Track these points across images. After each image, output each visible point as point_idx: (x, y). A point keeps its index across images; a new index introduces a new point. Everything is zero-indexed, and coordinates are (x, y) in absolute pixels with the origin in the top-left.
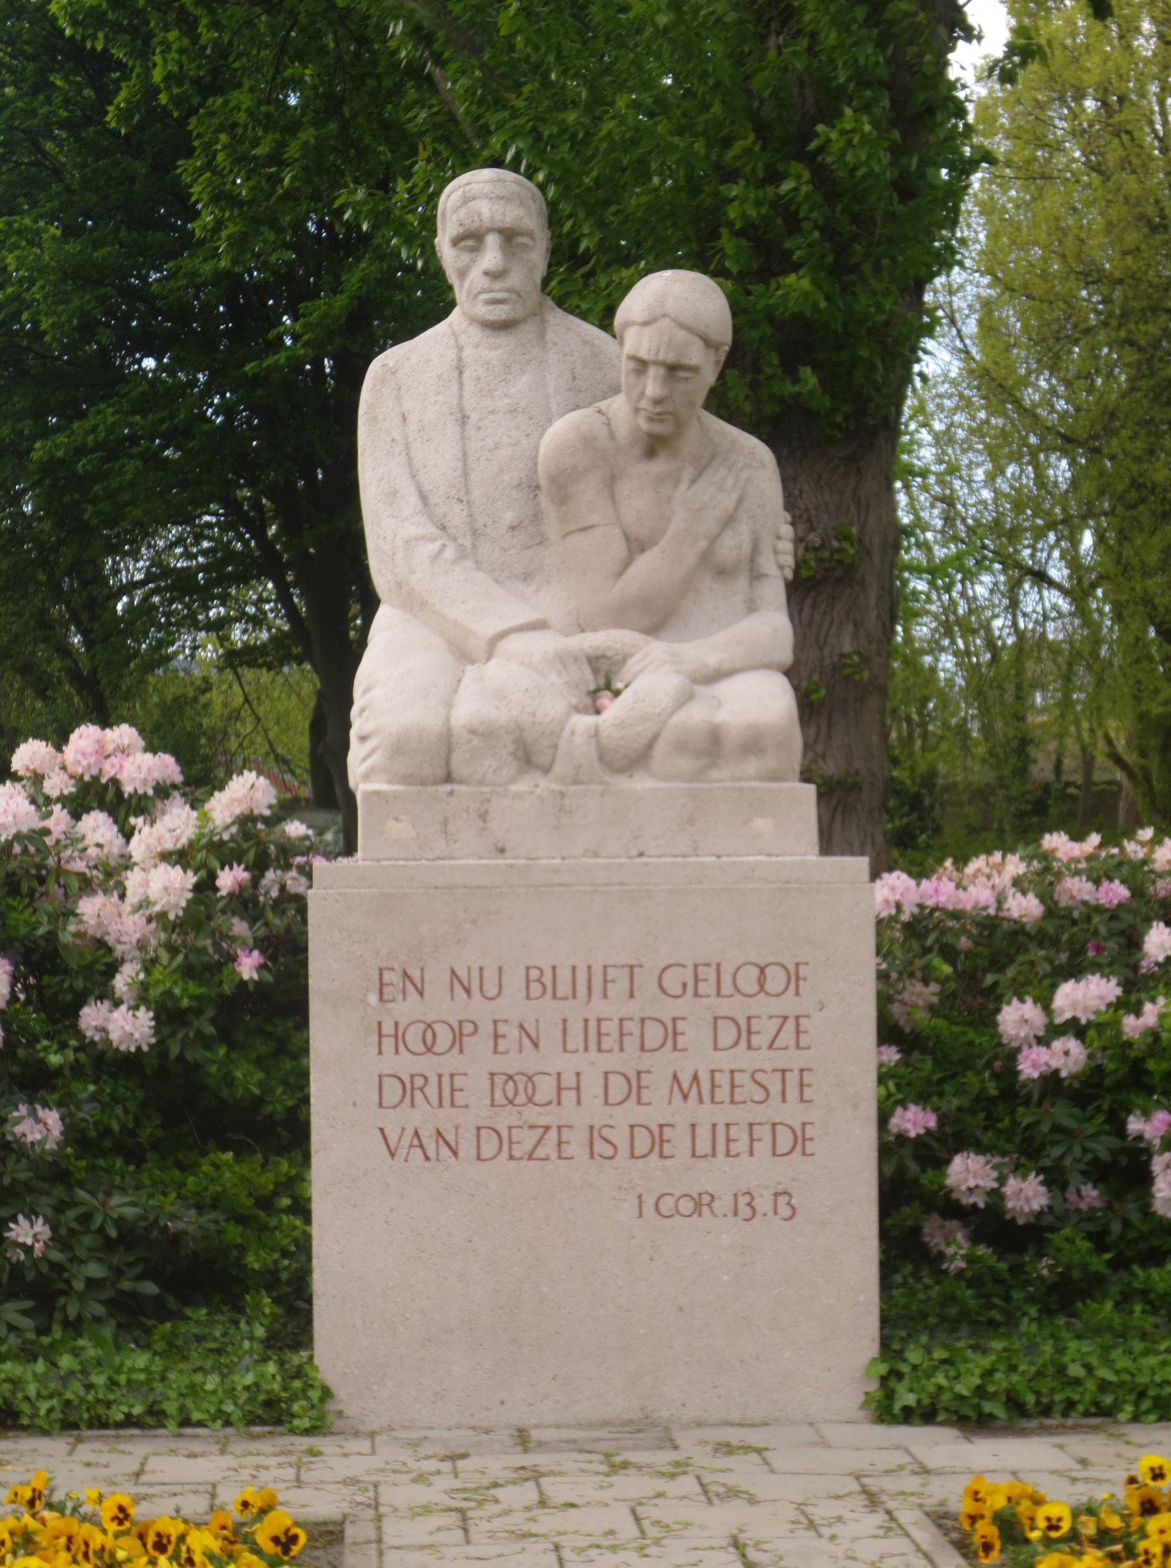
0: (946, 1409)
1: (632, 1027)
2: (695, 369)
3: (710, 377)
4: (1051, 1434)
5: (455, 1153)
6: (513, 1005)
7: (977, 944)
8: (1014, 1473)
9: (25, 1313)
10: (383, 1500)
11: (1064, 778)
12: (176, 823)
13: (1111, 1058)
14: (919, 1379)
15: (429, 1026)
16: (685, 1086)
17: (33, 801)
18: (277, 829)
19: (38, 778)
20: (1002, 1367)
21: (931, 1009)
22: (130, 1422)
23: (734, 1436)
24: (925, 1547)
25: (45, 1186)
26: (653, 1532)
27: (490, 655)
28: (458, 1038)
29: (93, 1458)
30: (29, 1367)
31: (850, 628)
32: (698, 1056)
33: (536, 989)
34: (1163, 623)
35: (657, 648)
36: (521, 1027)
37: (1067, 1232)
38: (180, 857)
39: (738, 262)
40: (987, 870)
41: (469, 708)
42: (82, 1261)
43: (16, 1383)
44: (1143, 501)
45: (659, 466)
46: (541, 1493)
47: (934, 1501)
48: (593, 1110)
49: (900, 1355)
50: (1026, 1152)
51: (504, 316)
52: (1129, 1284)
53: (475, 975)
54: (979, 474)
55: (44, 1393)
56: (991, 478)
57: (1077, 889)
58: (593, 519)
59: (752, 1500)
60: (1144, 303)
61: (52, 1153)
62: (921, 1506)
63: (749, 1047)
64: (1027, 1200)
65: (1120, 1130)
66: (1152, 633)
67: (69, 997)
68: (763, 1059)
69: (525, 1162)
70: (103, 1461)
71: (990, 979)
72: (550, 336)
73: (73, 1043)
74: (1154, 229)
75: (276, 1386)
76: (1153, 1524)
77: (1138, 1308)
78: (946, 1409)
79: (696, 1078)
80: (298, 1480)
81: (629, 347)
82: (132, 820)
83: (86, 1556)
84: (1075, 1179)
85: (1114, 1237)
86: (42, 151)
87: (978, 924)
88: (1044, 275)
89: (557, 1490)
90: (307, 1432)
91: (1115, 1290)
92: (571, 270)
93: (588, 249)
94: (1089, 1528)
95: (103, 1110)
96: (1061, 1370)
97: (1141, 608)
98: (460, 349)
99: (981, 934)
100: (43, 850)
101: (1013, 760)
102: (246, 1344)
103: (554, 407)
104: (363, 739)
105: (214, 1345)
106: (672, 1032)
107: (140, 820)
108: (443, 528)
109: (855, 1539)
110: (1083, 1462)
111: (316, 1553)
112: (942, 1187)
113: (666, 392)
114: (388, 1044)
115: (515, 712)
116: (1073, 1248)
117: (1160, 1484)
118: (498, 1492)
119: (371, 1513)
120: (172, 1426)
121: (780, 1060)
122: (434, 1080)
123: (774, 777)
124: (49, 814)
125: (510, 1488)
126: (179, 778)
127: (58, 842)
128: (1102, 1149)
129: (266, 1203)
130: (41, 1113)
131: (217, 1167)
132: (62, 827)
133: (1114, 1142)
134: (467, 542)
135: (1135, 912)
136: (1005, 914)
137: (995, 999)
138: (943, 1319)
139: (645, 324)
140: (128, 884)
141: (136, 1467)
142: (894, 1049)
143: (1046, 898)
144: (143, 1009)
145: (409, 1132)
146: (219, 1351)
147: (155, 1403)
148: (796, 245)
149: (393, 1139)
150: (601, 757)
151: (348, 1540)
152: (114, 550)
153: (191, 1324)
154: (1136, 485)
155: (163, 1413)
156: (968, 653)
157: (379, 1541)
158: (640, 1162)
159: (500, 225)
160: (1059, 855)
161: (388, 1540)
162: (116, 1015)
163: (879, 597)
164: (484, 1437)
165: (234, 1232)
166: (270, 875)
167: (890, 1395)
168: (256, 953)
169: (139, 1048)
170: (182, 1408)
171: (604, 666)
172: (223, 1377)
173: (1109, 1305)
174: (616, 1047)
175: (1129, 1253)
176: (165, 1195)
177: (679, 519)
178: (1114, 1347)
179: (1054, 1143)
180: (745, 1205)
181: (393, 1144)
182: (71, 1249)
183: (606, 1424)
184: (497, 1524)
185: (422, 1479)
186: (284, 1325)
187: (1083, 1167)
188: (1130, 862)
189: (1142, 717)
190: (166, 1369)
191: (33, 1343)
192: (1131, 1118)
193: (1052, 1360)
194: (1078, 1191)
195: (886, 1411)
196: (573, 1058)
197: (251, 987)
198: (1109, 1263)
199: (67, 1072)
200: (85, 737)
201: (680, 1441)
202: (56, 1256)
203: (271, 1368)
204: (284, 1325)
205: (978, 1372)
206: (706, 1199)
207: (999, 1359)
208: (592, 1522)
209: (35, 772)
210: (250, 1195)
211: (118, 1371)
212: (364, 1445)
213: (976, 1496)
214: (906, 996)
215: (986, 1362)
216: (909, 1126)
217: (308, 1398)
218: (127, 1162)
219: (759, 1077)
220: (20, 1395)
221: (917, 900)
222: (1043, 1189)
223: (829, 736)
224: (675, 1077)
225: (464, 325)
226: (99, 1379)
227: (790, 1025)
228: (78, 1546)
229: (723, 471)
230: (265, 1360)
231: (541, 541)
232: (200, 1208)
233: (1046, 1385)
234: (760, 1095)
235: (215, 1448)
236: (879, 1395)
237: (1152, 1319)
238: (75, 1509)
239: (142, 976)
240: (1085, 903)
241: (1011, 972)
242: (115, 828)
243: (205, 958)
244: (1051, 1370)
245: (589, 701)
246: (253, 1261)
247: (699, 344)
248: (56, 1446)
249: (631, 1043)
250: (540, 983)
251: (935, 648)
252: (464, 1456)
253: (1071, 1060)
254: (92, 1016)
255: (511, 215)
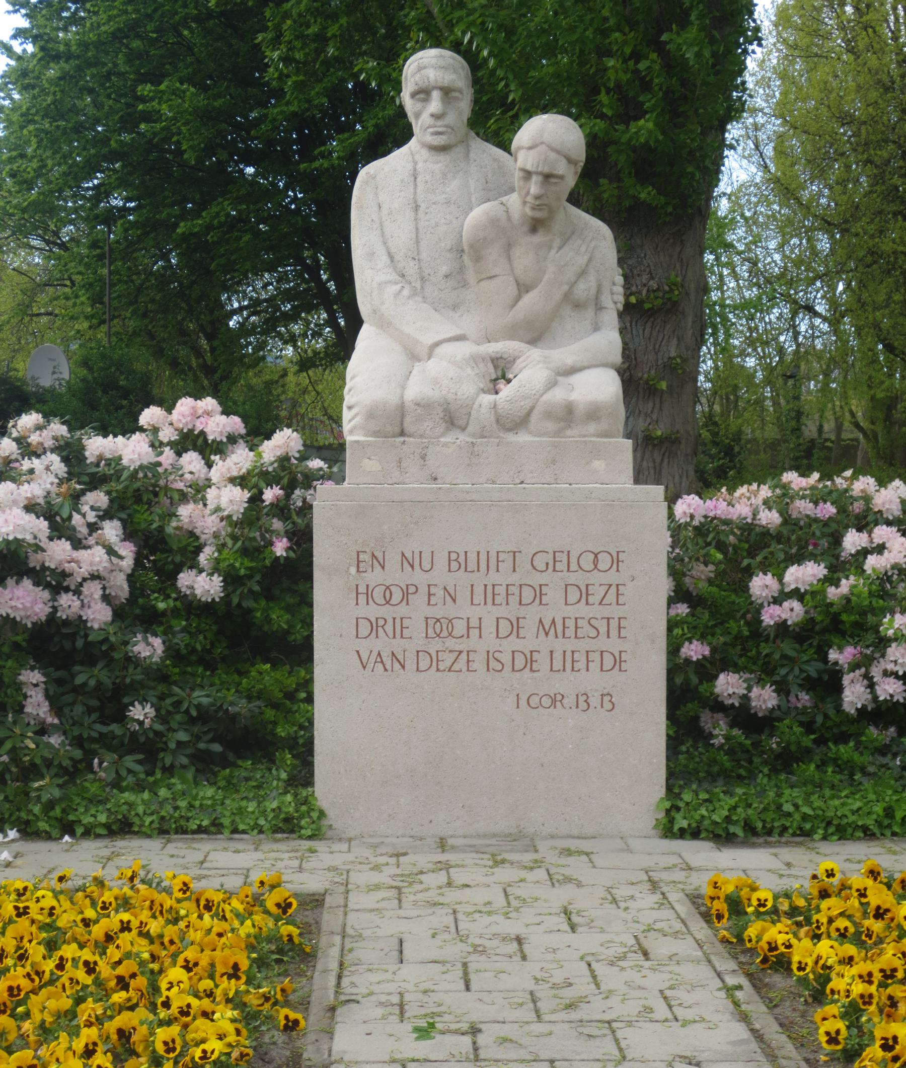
0: (707, 830)
1: (514, 590)
2: (561, 177)
3: (571, 181)
4: (772, 847)
5: (403, 667)
6: (440, 576)
7: (740, 541)
8: (744, 871)
9: (139, 762)
10: (351, 880)
11: (825, 436)
12: (240, 459)
13: (820, 613)
14: (689, 811)
15: (388, 587)
16: (547, 627)
17: (152, 445)
18: (304, 463)
19: (155, 430)
20: (742, 805)
21: (710, 582)
22: (201, 830)
23: (573, 844)
24: (683, 916)
25: (152, 684)
26: (515, 903)
28: (406, 595)
29: (175, 852)
30: (140, 795)
31: (675, 341)
32: (555, 609)
33: (454, 566)
34: (886, 339)
35: (535, 353)
36: (445, 589)
37: (787, 722)
38: (241, 481)
39: (611, 108)
40: (748, 495)
41: (415, 390)
42: (174, 731)
43: (131, 805)
44: (875, 262)
45: (538, 238)
46: (449, 878)
47: (692, 887)
48: (489, 642)
49: (678, 796)
50: (766, 671)
51: (443, 143)
52: (826, 755)
53: (417, 557)
54: (772, 245)
55: (148, 812)
56: (780, 248)
57: (803, 507)
58: (497, 271)
59: (579, 885)
60: (879, 137)
61: (156, 663)
62: (683, 890)
63: (587, 604)
64: (765, 701)
65: (825, 659)
66: (880, 347)
67: (171, 567)
68: (596, 611)
69: (446, 673)
70: (182, 854)
71: (746, 562)
72: (472, 155)
73: (174, 595)
74: (887, 89)
75: (291, 809)
76: (824, 904)
77: (830, 770)
78: (707, 830)
79: (553, 621)
80: (300, 867)
81: (520, 163)
82: (213, 457)
83: (161, 912)
84: (794, 689)
85: (818, 725)
86: (180, 35)
87: (739, 529)
88: (817, 118)
89: (459, 876)
90: (310, 838)
91: (817, 758)
92: (504, 113)
93: (514, 100)
94: (784, 906)
95: (191, 637)
96: (779, 807)
97: (872, 331)
98: (415, 163)
99: (742, 534)
100: (157, 475)
101: (793, 423)
102: (275, 783)
103: (473, 200)
104: (350, 408)
105: (254, 784)
106: (539, 594)
107: (218, 457)
108: (403, 276)
109: (640, 910)
110: (788, 865)
111: (307, 913)
112: (712, 694)
113: (543, 191)
114: (362, 599)
115: (444, 392)
116: (792, 731)
117: (831, 880)
118: (422, 877)
119: (342, 889)
120: (227, 832)
121: (607, 612)
122: (390, 621)
123: (606, 435)
124: (161, 453)
125: (430, 874)
126: (243, 431)
127: (166, 470)
128: (812, 670)
129: (291, 696)
130: (151, 639)
131: (261, 673)
132: (170, 461)
133: (820, 666)
134: (418, 285)
135: (838, 523)
136: (757, 522)
137: (749, 573)
138: (708, 773)
139: (530, 148)
140: (208, 496)
141: (201, 858)
142: (685, 605)
143: (784, 513)
144: (216, 575)
145: (375, 654)
146: (259, 787)
147: (216, 819)
148: (648, 101)
149: (365, 657)
150: (498, 421)
151: (327, 905)
152: (226, 289)
153: (242, 770)
154: (872, 253)
155: (221, 825)
156: (764, 357)
157: (346, 906)
158: (518, 674)
159: (440, 84)
160: (793, 486)
161: (351, 905)
162: (199, 578)
163: (694, 322)
164: (419, 842)
165: (270, 714)
166: (297, 492)
167: (671, 821)
168: (285, 540)
169: (213, 599)
170: (233, 822)
171: (501, 364)
172: (259, 803)
173: (812, 767)
174: (504, 602)
175: (827, 735)
176: (228, 690)
177: (551, 271)
178: (813, 793)
179: (782, 666)
180: (583, 702)
181: (364, 661)
182: (168, 723)
183: (494, 835)
184: (420, 896)
185: (377, 868)
186: (300, 772)
187: (801, 682)
188: (837, 490)
189: (873, 398)
190: (225, 798)
191: (143, 780)
192: (831, 651)
193: (773, 801)
194: (797, 696)
195: (669, 831)
196: (478, 608)
197: (282, 561)
198: (815, 741)
199: (169, 613)
200: (185, 405)
201: (540, 847)
202: (158, 727)
203: (289, 798)
204: (300, 772)
205: (727, 807)
206: (559, 697)
207: (740, 800)
208: (478, 896)
209: (153, 426)
210: (281, 691)
211: (195, 799)
212: (344, 846)
213: (715, 885)
214: (694, 573)
215: (732, 801)
216: (692, 653)
217: (310, 817)
218: (206, 670)
219: (593, 622)
220: (133, 813)
221: (704, 513)
222: (774, 695)
223: (661, 409)
224: (541, 621)
225: (419, 148)
226: (183, 804)
227: (613, 590)
228: (157, 907)
229: (579, 242)
230: (286, 792)
231: (465, 285)
232: (249, 698)
233: (769, 816)
234: (593, 633)
235: (252, 847)
236: (665, 820)
237: (838, 777)
238: (158, 884)
239: (216, 554)
240: (808, 516)
241: (759, 558)
242: (203, 462)
243: (255, 544)
244: (773, 807)
245: (491, 386)
246: (281, 731)
247: (564, 161)
248: (155, 844)
249: (514, 600)
251: (743, 354)
252: (405, 854)
253: (794, 614)
254: (185, 579)
255: (448, 78)
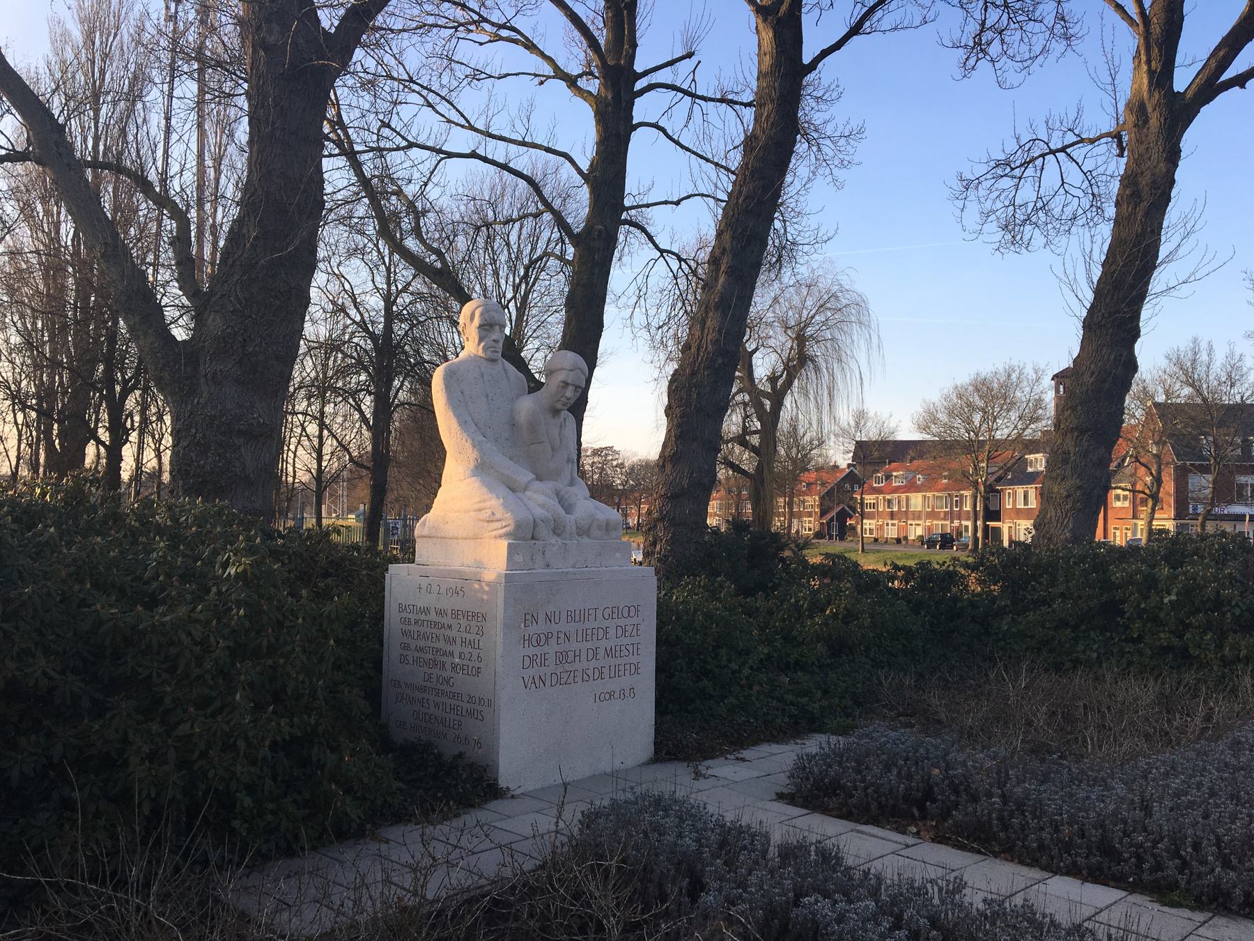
6: (563, 626)
27: (525, 489)
250: (571, 617)
